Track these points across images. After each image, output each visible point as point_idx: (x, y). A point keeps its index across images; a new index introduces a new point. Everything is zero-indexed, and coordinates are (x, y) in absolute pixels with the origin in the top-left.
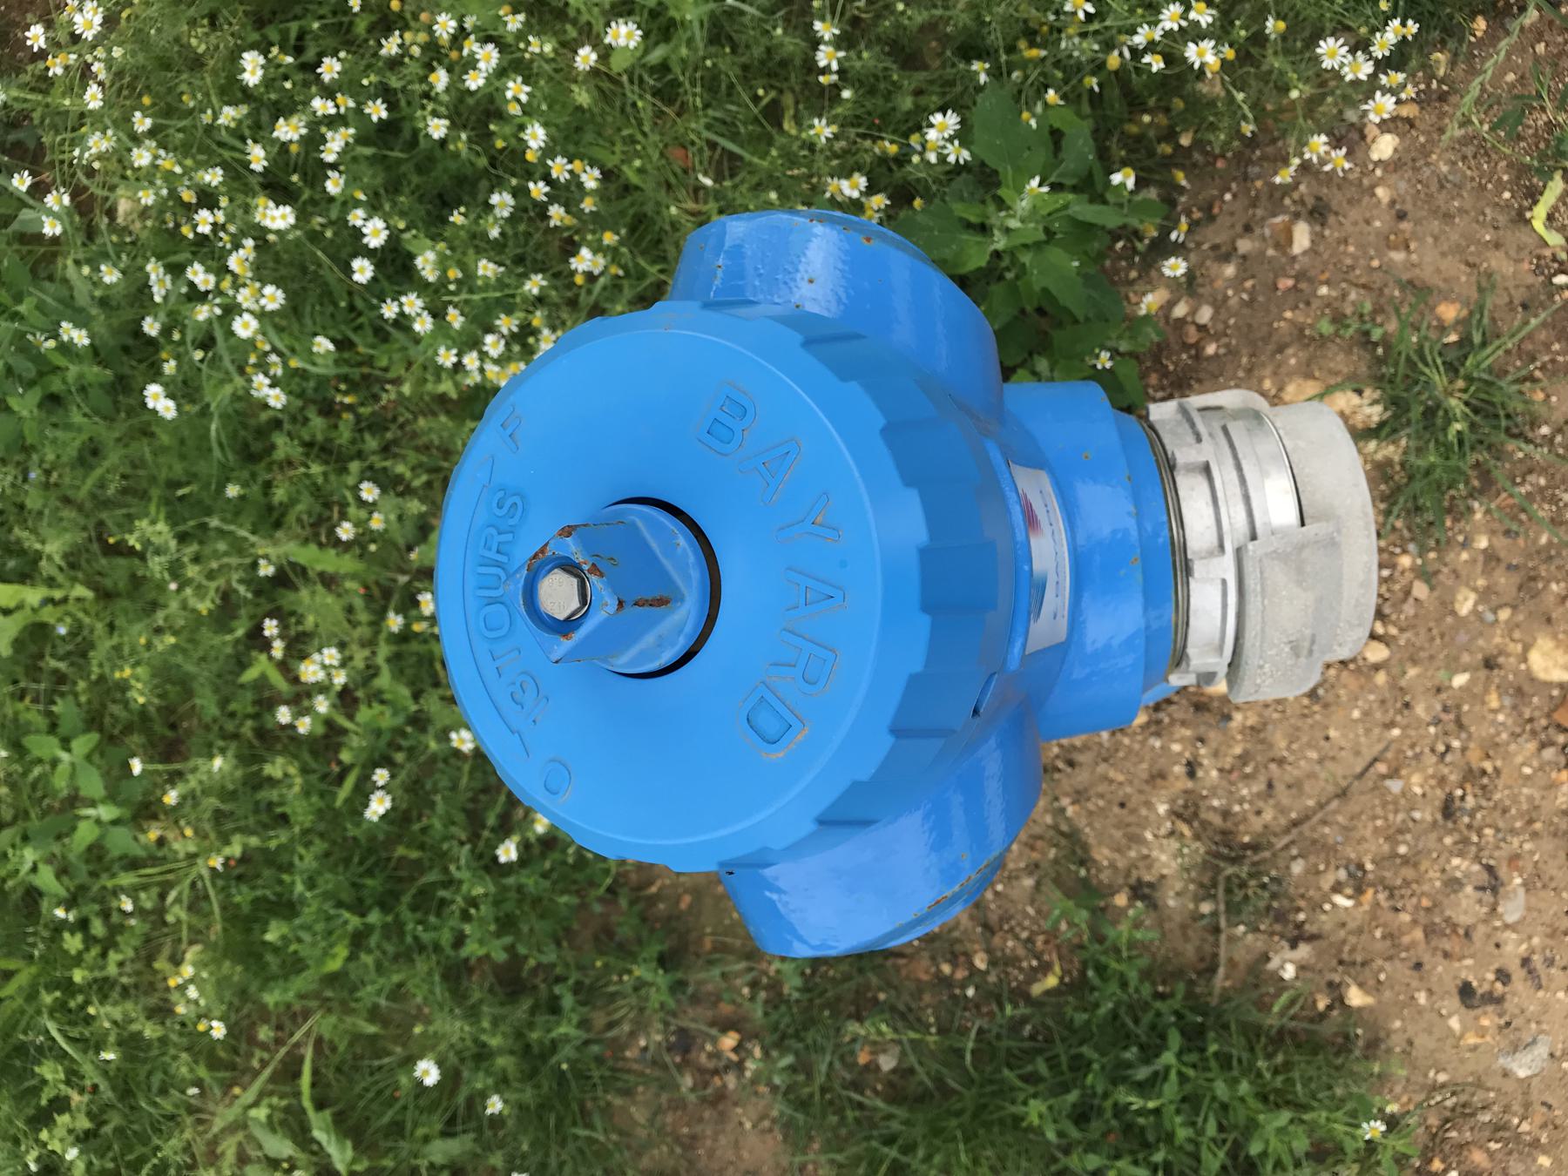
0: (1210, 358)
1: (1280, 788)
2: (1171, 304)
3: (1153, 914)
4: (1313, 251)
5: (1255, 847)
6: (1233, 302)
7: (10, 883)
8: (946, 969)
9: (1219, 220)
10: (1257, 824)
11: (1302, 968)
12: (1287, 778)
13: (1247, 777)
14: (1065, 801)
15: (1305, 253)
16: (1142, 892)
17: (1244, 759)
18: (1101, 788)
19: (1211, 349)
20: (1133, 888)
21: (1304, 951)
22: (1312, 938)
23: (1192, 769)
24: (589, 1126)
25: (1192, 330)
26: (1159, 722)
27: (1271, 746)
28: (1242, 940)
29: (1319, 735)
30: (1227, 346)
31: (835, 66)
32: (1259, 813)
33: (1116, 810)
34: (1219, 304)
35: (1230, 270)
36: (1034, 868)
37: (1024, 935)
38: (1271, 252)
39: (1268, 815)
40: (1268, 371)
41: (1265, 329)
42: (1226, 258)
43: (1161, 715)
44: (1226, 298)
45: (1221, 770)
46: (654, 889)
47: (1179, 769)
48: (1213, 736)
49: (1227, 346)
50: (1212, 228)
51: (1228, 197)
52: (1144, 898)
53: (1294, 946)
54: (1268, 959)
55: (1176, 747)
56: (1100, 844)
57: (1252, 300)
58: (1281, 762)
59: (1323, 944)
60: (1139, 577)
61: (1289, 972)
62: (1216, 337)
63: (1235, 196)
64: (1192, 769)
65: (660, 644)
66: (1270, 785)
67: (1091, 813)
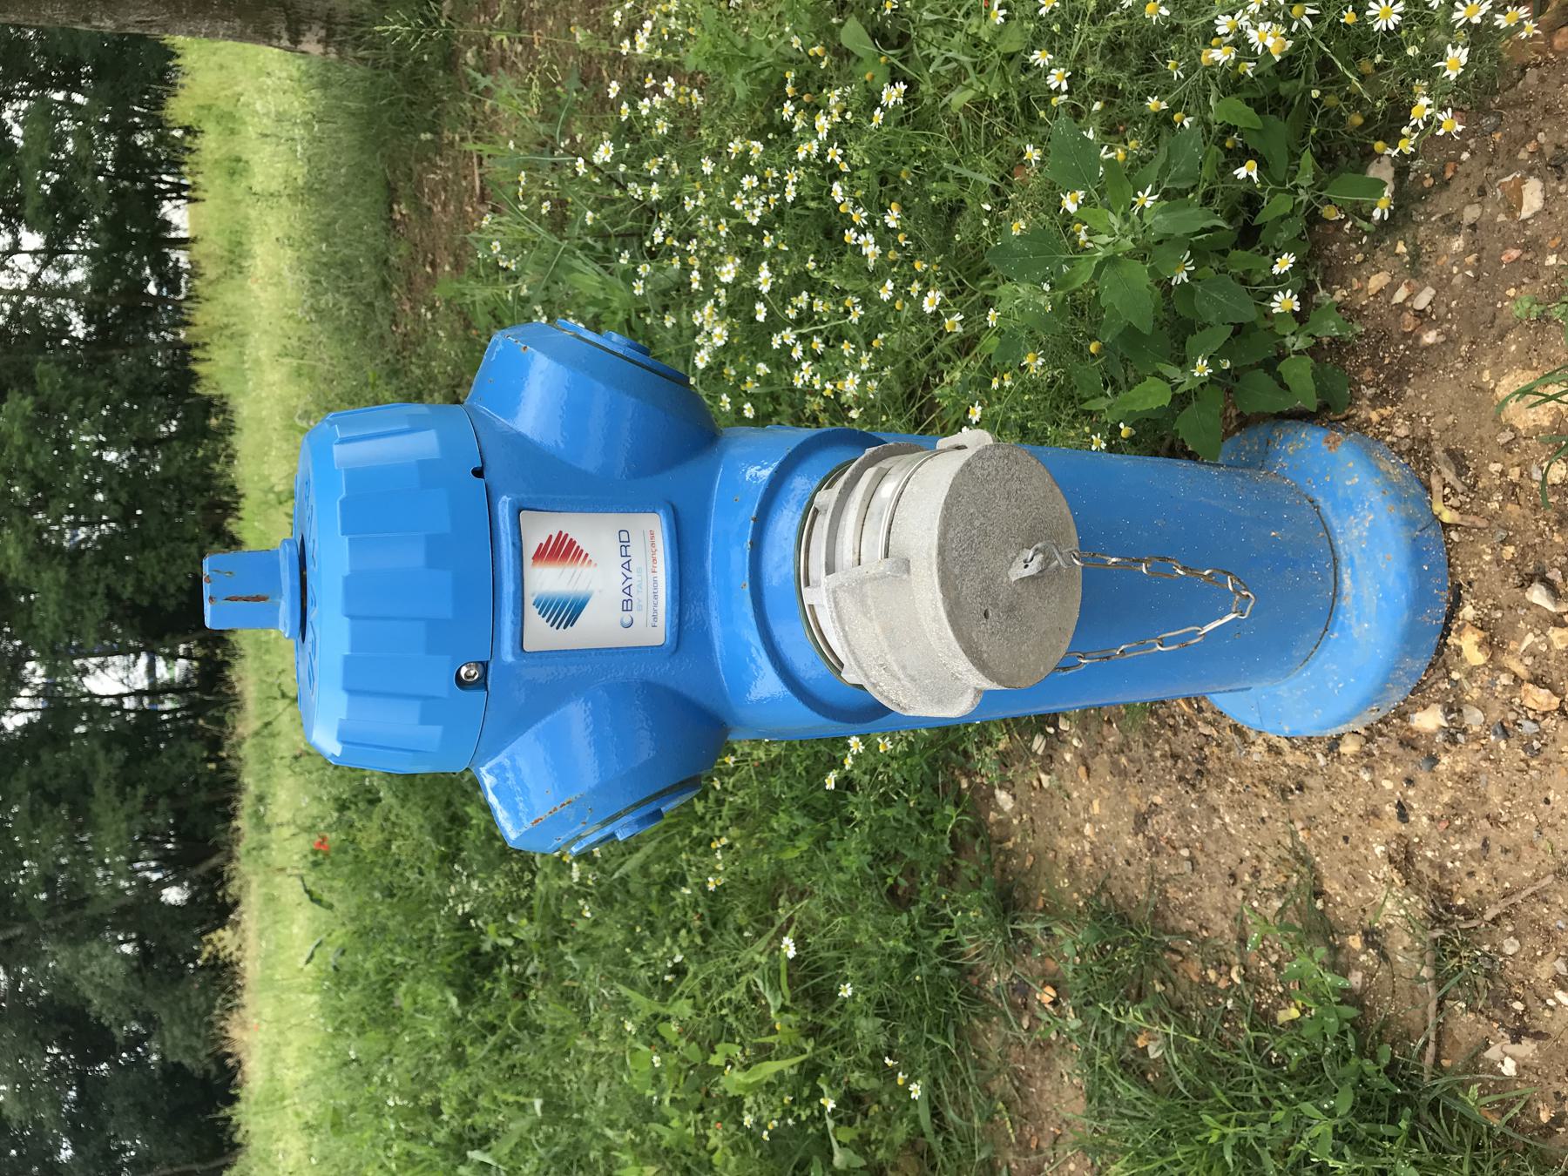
0: (1428, 348)
1: (1495, 850)
2: (1393, 288)
3: (1385, 966)
4: (1546, 211)
5: (1468, 914)
6: (1457, 280)
7: (40, 706)
8: (1212, 975)
9: (1453, 185)
10: (1471, 887)
11: (1522, 1067)
12: (1505, 841)
13: (1460, 830)
14: (1299, 825)
15: (1536, 215)
16: (1371, 938)
17: (1455, 807)
18: (1327, 818)
19: (1430, 338)
20: (1366, 933)
21: (1527, 1048)
22: (1538, 1036)
23: (1403, 812)
24: (946, 1039)
25: (1408, 317)
26: (1370, 754)
27: (1485, 800)
28: (1465, 1023)
29: (1537, 795)
30: (1447, 333)
31: (1065, 87)
32: (1471, 874)
33: (1341, 842)
34: (1443, 284)
35: (1458, 244)
36: (1282, 891)
37: (1274, 958)
38: (1501, 218)
39: (1482, 879)
40: (1486, 362)
41: (1489, 310)
42: (1454, 229)
43: (1373, 747)
44: (1451, 275)
45: (1432, 818)
46: (1010, 845)
47: (1390, 809)
48: (1423, 777)
49: (1447, 333)
50: (1445, 195)
51: (1465, 156)
52: (1374, 945)
53: (1516, 1040)
54: (1487, 1046)
55: (1388, 785)
56: (1332, 878)
57: (1477, 278)
58: (1494, 820)
59: (1548, 1045)
60: (1079, 596)
61: (1509, 1068)
62: (1433, 324)
63: (1472, 153)
64: (1403, 812)
65: (936, 619)
66: (1485, 844)
67: (1319, 841)
